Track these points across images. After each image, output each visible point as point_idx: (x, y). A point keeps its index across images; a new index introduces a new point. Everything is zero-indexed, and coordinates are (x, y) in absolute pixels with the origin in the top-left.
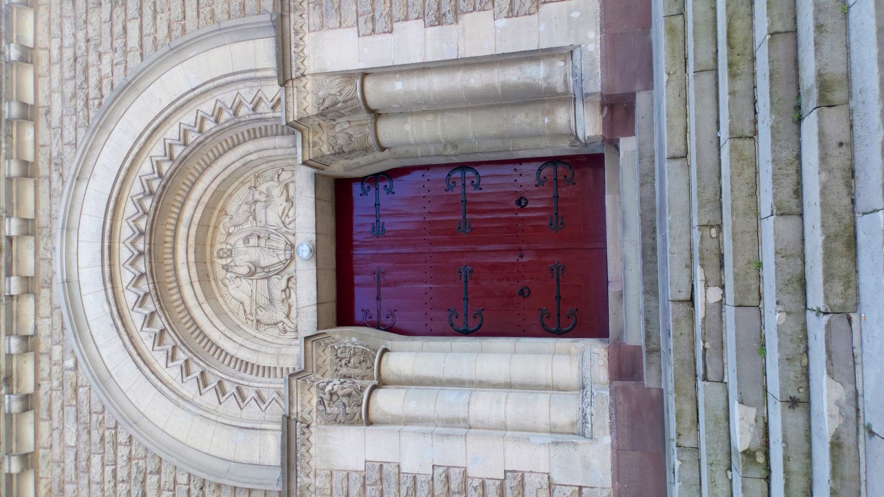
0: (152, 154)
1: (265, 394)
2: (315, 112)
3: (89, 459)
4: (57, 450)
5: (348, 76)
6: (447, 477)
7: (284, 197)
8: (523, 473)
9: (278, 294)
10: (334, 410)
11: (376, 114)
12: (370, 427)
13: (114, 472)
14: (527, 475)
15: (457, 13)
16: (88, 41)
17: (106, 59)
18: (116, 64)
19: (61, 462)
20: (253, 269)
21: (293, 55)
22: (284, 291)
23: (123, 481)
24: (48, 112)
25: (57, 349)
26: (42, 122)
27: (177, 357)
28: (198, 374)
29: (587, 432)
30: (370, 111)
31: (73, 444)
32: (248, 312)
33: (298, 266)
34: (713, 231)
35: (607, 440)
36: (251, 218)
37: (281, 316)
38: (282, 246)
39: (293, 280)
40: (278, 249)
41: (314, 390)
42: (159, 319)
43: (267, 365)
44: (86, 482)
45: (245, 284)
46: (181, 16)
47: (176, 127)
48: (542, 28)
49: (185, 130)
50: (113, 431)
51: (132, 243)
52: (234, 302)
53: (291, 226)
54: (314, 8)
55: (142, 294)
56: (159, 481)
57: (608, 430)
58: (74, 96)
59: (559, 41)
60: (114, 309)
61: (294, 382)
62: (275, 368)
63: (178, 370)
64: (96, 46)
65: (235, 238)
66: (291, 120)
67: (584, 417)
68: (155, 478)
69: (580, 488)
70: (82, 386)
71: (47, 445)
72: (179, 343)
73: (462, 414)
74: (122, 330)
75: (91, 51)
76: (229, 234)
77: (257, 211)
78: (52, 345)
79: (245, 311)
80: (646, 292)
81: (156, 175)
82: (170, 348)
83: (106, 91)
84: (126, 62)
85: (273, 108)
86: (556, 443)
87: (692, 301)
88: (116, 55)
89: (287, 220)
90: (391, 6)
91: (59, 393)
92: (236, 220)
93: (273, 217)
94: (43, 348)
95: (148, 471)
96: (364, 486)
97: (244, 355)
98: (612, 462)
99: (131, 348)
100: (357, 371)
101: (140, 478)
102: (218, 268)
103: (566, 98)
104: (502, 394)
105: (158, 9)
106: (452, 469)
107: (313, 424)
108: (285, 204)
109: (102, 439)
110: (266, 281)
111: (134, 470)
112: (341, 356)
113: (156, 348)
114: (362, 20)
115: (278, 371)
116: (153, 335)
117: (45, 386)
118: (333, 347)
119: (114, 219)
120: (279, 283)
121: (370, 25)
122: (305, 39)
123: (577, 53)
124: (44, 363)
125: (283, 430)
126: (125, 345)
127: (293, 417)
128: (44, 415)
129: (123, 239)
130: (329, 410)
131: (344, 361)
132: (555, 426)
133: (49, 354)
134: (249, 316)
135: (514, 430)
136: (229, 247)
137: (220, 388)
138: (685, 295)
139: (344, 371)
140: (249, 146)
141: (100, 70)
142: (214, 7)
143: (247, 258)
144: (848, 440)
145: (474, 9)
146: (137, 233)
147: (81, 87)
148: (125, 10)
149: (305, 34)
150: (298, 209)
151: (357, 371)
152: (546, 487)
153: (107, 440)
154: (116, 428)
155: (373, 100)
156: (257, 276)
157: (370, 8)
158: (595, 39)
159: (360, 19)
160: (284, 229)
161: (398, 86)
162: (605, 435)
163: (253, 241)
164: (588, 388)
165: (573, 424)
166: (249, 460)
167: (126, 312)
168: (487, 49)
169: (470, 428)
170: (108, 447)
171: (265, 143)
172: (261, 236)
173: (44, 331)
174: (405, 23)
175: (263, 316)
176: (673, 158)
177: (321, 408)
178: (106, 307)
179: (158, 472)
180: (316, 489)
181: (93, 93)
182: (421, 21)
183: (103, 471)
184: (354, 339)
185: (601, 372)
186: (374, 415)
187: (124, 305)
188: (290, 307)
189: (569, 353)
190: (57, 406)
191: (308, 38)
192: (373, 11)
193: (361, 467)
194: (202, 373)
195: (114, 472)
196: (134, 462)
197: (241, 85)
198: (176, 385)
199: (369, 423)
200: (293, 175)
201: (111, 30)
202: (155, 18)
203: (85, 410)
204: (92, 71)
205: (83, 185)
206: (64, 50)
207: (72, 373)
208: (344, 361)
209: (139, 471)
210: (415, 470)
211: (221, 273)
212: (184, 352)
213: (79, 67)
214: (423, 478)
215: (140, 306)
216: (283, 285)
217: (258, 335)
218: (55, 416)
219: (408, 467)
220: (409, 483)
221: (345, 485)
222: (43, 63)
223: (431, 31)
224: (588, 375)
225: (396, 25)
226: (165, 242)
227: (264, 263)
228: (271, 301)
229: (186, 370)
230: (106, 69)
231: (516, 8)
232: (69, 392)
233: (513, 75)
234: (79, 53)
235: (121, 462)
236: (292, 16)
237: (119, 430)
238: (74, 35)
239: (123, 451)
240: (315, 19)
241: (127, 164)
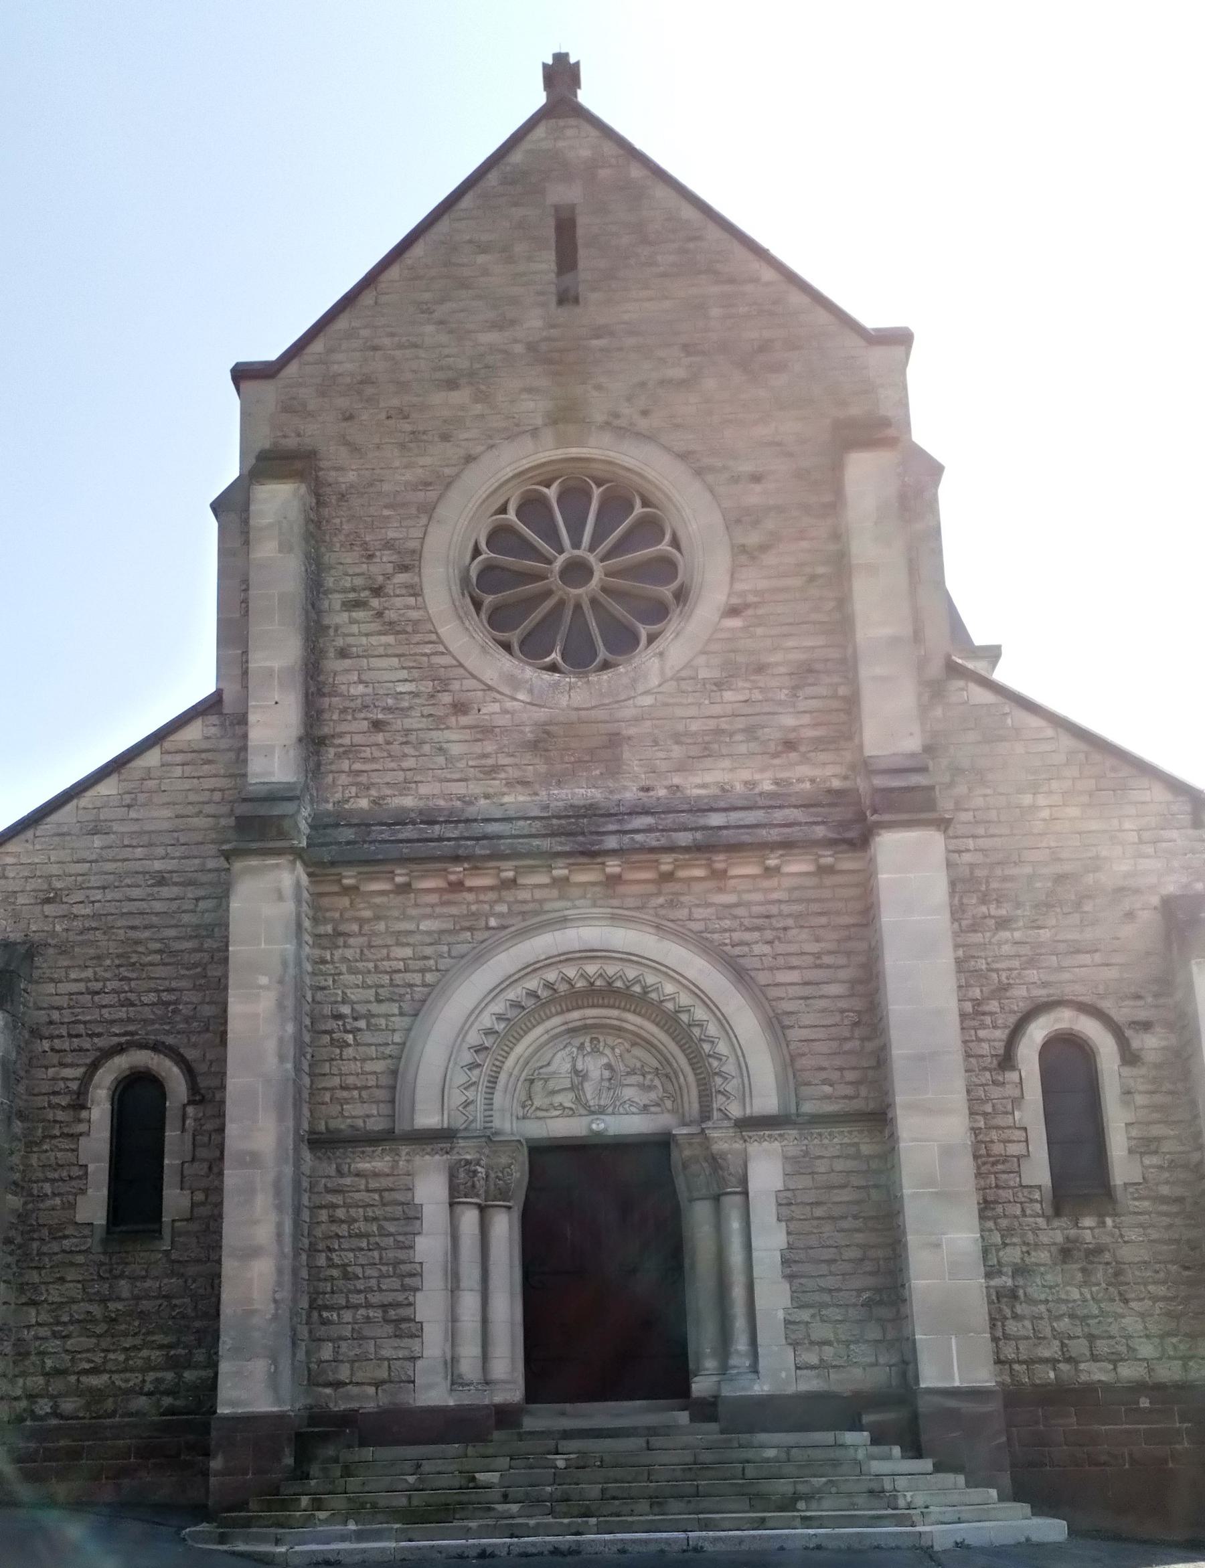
0: (681, 994)
1: (471, 1108)
3: (408, 944)
4: (413, 912)
5: (744, 1181)
6: (414, 1275)
7: (647, 1102)
11: (717, 1199)
13: (399, 971)
15: (790, 1277)
16: (785, 929)
17: (766, 949)
19: (405, 917)
22: (561, 1104)
23: (391, 980)
27: (501, 1022)
30: (719, 1196)
31: (421, 927)
32: (541, 1071)
34: (599, 1463)
35: (451, 1403)
37: (537, 1103)
38: (602, 1103)
39: (571, 1113)
40: (600, 1099)
41: (477, 1156)
44: (389, 943)
46: (801, 1024)
47: (705, 1018)
49: (702, 1025)
51: (601, 975)
53: (621, 1110)
54: (802, 1151)
55: (555, 987)
56: (393, 1015)
58: (735, 917)
59: (762, 1363)
61: (483, 1139)
63: (489, 1025)
64: (779, 938)
67: (468, 1385)
68: (396, 1011)
69: (413, 1382)
70: (472, 934)
73: (463, 1284)
74: (523, 973)
75: (774, 933)
76: (613, 1049)
80: (565, 1431)
82: (508, 1016)
84: (763, 970)
86: (446, 1363)
90: (801, 1220)
91: (465, 912)
92: (626, 1056)
93: (628, 1093)
94: (504, 893)
95: (402, 1004)
96: (403, 1204)
102: (581, 1040)
103: (724, 1369)
105: (809, 1002)
106: (419, 1278)
107: (449, 1157)
109: (426, 958)
111: (402, 991)
114: (789, 1194)
115: (490, 1113)
116: (519, 999)
117: (470, 897)
118: (512, 1164)
120: (566, 1099)
121: (784, 1202)
124: (491, 896)
126: (510, 976)
127: (455, 1140)
128: (446, 897)
129: (605, 967)
131: (500, 1175)
132: (458, 1361)
133: (500, 900)
134: (537, 1072)
136: (601, 1049)
137: (473, 1066)
139: (493, 1175)
140: (691, 1078)
141: (757, 942)
143: (591, 1067)
144: (492, 1514)
145: (793, 1292)
150: (640, 1116)
151: (492, 1187)
154: (437, 970)
155: (726, 1200)
157: (799, 1201)
158: (762, 1391)
160: (618, 1103)
162: (455, 1401)
163: (607, 1074)
165: (460, 1376)
168: (760, 1303)
169: (452, 1291)
171: (694, 1093)
172: (613, 1078)
173: (524, 895)
174: (784, 1232)
175: (538, 1085)
176: (648, 1442)
179: (401, 1014)
180: (397, 1162)
181: (737, 936)
184: (518, 1175)
186: (459, 1209)
187: (545, 970)
188: (547, 1110)
190: (454, 910)
191: (776, 1145)
192: (797, 1204)
193: (417, 1201)
194: (487, 1048)
195: (399, 971)
196: (408, 990)
197: (740, 1080)
198: (477, 1026)
199: (451, 1205)
200: (668, 1111)
201: (793, 954)
203: (451, 939)
204: (756, 935)
207: (483, 924)
208: (500, 1175)
209: (401, 995)
210: (418, 1247)
212: (504, 1028)
213: (759, 922)
214: (412, 1255)
217: (520, 1083)
218: (445, 910)
222: (767, 884)
223: (778, 1254)
224: (498, 1387)
225: (784, 1224)
227: (586, 1085)
230: (758, 949)
232: (467, 924)
234: (774, 921)
235: (408, 976)
238: (790, 915)
240: (792, 1151)
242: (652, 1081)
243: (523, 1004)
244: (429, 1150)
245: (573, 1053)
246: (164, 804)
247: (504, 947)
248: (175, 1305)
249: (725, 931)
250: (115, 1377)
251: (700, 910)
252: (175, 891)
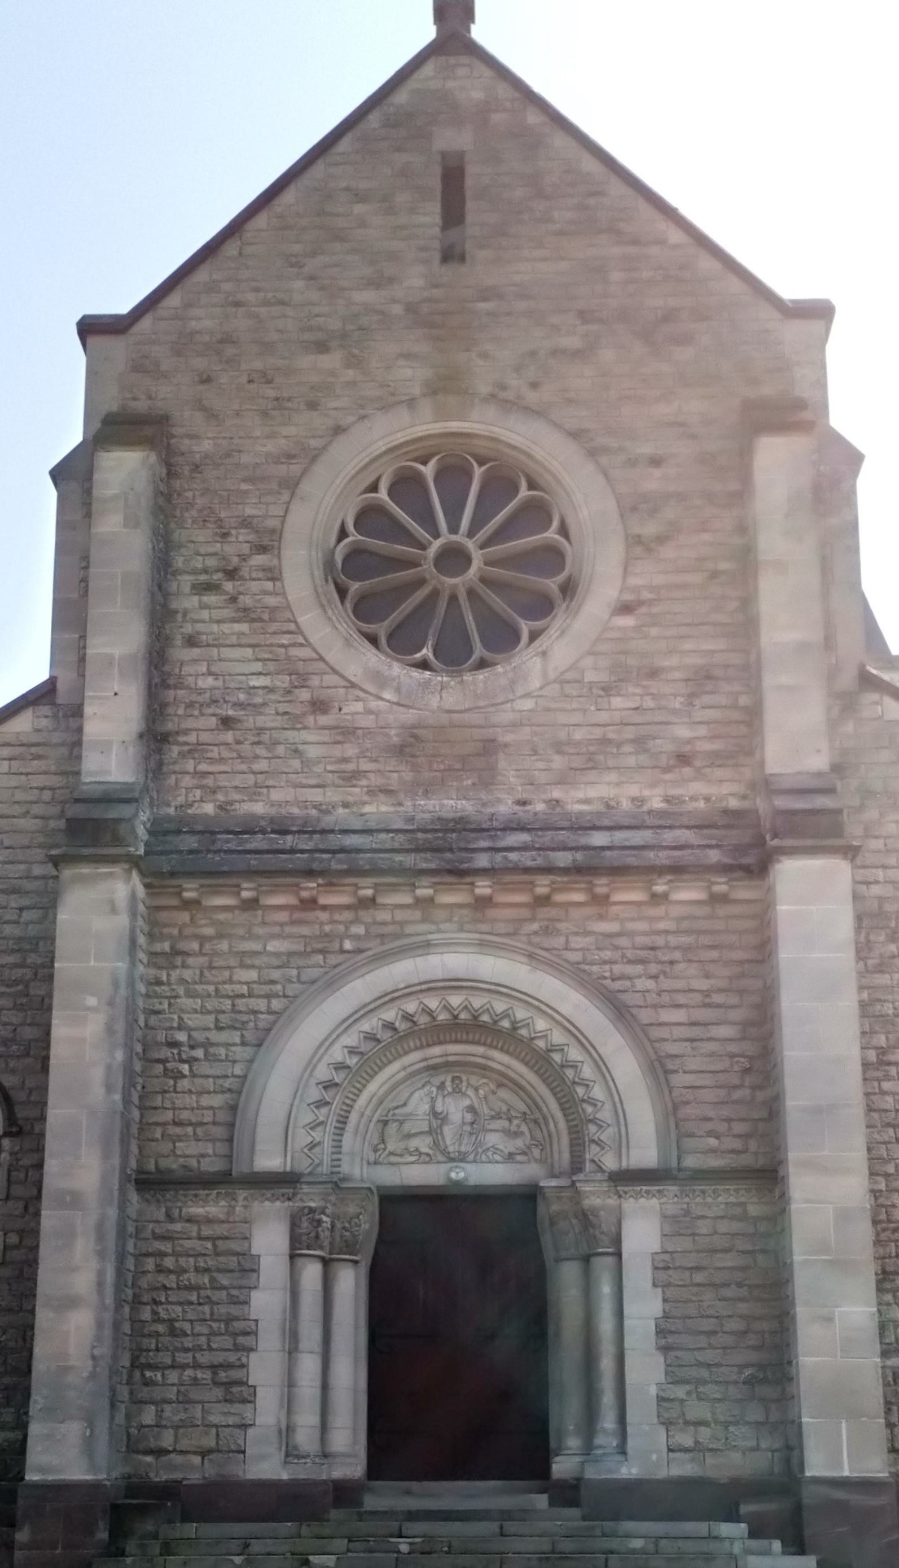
0: (554, 1030)
1: (317, 1150)
4: (260, 931)
5: (617, 1241)
6: (248, 1334)
7: (513, 1150)
8: (253, 1402)
9: (414, 1143)
10: (305, 1224)
11: (586, 1260)
12: (288, 1257)
13: (242, 996)
14: (252, 1405)
16: (672, 963)
17: (650, 984)
18: (644, 996)
19: (251, 936)
20: (441, 1116)
21: (639, 1188)
23: (233, 1005)
24: (601, 917)
27: (353, 1056)
28: (337, 1080)
29: (290, 1459)
31: (268, 948)
32: (396, 1111)
34: (446, 1549)
35: (285, 1476)
36: (493, 1113)
38: (463, 1149)
39: (428, 1159)
40: (460, 1145)
41: (322, 1204)
43: (344, 1143)
45: (426, 1107)
46: (687, 1069)
47: (580, 1058)
48: (646, 1428)
49: (576, 1067)
50: (281, 994)
52: (404, 1096)
54: (682, 1209)
55: (415, 1019)
56: (234, 1045)
57: (292, 1477)
58: (617, 948)
59: (631, 1443)
60: (400, 993)
61: (330, 1185)
63: (340, 1059)
64: (665, 973)
67: (304, 1457)
68: (238, 1040)
69: (244, 1452)
70: (325, 958)
71: (267, 919)
72: (366, 1057)
75: (660, 967)
76: (476, 1089)
78: (365, 924)
79: (396, 1108)
80: (410, 1512)
81: (533, 1035)
82: (362, 1050)
84: (646, 1007)
85: (593, 1161)
86: (280, 1432)
87: (401, 1537)
88: (654, 996)
89: (490, 1154)
91: (318, 933)
92: (491, 1097)
94: (362, 913)
95: (244, 1032)
96: (238, 1254)
97: (354, 1117)
99: (362, 1012)
100: (338, 1239)
101: (237, 1025)
102: (442, 1078)
103: (588, 1448)
104: (318, 1383)
105: (695, 1044)
107: (291, 1203)
108: (506, 1151)
109: (273, 982)
110: (427, 1129)
112: (353, 1224)
113: (362, 1035)
117: (324, 916)
118: (361, 1213)
119: (489, 991)
120: (423, 1144)
121: (661, 1265)
123: (622, 1458)
124: (347, 915)
126: (365, 1006)
127: (298, 1185)
128: (297, 915)
130: (304, 1218)
131: (347, 1225)
132: (294, 1431)
133: (357, 921)
134: (391, 1113)
135: (289, 1392)
136: (464, 1089)
137: (321, 1104)
139: (339, 1225)
140: (562, 1124)
141: (640, 977)
143: (452, 1110)
146: (476, 1014)
147: (623, 956)
151: (338, 1239)
152: (243, 1422)
153: (272, 987)
154: (285, 996)
156: (433, 1121)
157: (677, 1264)
158: (630, 1474)
160: (480, 1150)
161: (606, 1289)
163: (469, 1117)
164: (325, 1461)
165: (296, 1448)
167: (398, 1002)
170: (266, 989)
171: (565, 1141)
172: (476, 1123)
175: (393, 1127)
177: (306, 1211)
178: (402, 985)
179: (243, 1044)
180: (234, 1207)
181: (617, 969)
183: (243, 983)
187: (403, 1000)
188: (401, 1155)
190: (305, 930)
191: (654, 1202)
192: (675, 1268)
193: (254, 1252)
194: (336, 1085)
195: (242, 996)
196: (252, 1017)
197: (616, 1129)
198: (327, 1059)
199: (292, 1257)
202: (687, 1040)
203: (301, 962)
204: (639, 968)
205: (524, 960)
207: (337, 946)
209: (244, 1023)
211: (437, 1081)
212: (357, 1063)
217: (372, 1124)
220: (242, 1298)
221: (238, 1235)
223: (653, 1324)
225: (659, 1290)
226: (467, 1033)
228: (409, 1136)
229: (340, 1067)
230: (641, 984)
231: (665, 1404)
233: (608, 1399)
234: (659, 953)
237: (282, 999)
238: (677, 948)
239: (261, 1004)
241: (544, 1007)
242: (518, 1126)
243: (379, 1036)
244: (269, 1195)
245: (432, 1092)
249: (605, 962)
251: (579, 939)
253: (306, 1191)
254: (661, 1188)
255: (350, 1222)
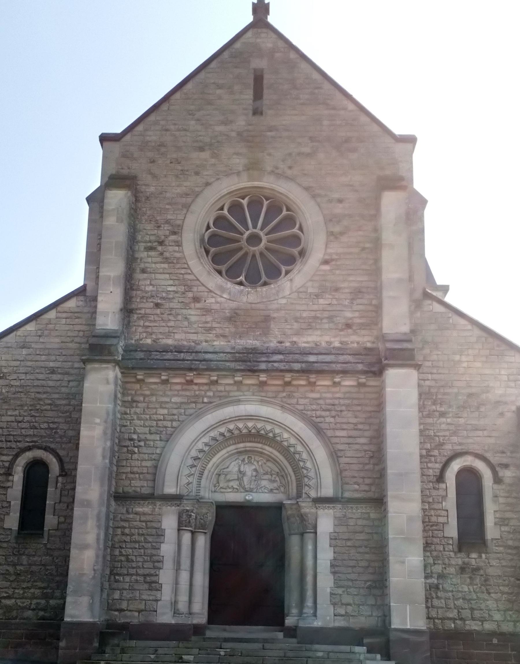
1: (190, 486)
2: (302, 513)
3: (165, 408)
4: (169, 393)
5: (315, 527)
8: (161, 590)
9: (231, 484)
10: (184, 516)
11: (302, 535)
13: (161, 420)
14: (160, 592)
15: (334, 573)
16: (341, 411)
17: (332, 420)
19: (165, 395)
20: (242, 473)
21: (325, 505)
23: (157, 424)
24: (312, 391)
25: (210, 394)
26: (307, 388)
30: (303, 533)
32: (224, 470)
33: (243, 493)
34: (240, 654)
35: (173, 622)
36: (265, 472)
37: (221, 485)
38: (252, 487)
39: (237, 491)
40: (250, 485)
41: (192, 508)
42: (222, 438)
43: (202, 483)
45: (236, 469)
47: (301, 450)
48: (325, 606)
49: (300, 454)
50: (177, 420)
54: (343, 514)
55: (233, 432)
56: (157, 440)
57: (176, 622)
58: (318, 404)
59: (319, 612)
60: (227, 421)
62: (200, 487)
63: (201, 448)
64: (338, 415)
65: (256, 465)
66: (299, 503)
67: (181, 614)
68: (158, 439)
69: (156, 611)
70: (196, 405)
71: (172, 388)
73: (182, 568)
74: (218, 424)
75: (336, 413)
76: (258, 462)
77: (268, 476)
79: (224, 469)
80: (225, 638)
81: (282, 440)
82: (210, 444)
83: (318, 420)
84: (330, 429)
87: (221, 649)
88: (334, 425)
89: (263, 489)
90: (340, 547)
92: (264, 465)
94: (212, 387)
96: (156, 528)
98: (165, 623)
102: (243, 457)
103: (301, 613)
105: (350, 445)
106: (162, 563)
108: (270, 488)
109: (174, 415)
110: (237, 478)
112: (205, 517)
114: (336, 534)
116: (216, 437)
117: (196, 387)
118: (208, 513)
120: (235, 484)
121: (333, 538)
122: (331, 510)
123: (314, 618)
124: (206, 388)
125: (177, 495)
126: (212, 426)
127: (182, 500)
128: (184, 387)
131: (202, 517)
132: (177, 603)
133: (210, 390)
134: (222, 471)
136: (253, 462)
137: (193, 466)
138: (222, 648)
139: (199, 517)
140: (293, 478)
141: (328, 417)
142: (349, 470)
143: (247, 470)
146: (259, 430)
148: (352, 430)
149: (333, 510)
150: (269, 494)
151: (198, 523)
152: (156, 599)
153: (173, 417)
154: (179, 421)
158: (318, 625)
159: (336, 534)
160: (259, 488)
161: (310, 547)
163: (254, 473)
164: (190, 616)
165: (178, 610)
166: (166, 480)
167: (226, 425)
171: (295, 485)
173: (221, 388)
175: (222, 477)
176: (263, 646)
177: (185, 511)
178: (228, 418)
179: (161, 440)
180: (155, 509)
181: (318, 413)
182: (333, 558)
185: (196, 621)
187: (228, 424)
188: (225, 489)
189: (203, 609)
190: (188, 393)
191: (331, 511)
192: (339, 539)
193: (163, 527)
194: (199, 458)
195: (161, 420)
196: (165, 429)
197: (316, 480)
198: (195, 448)
199: (179, 530)
202: (347, 444)
205: (279, 408)
206: (338, 400)
209: (161, 431)
210: (162, 549)
212: (208, 450)
213: (329, 407)
215: (228, 430)
216: (235, 487)
217: (214, 476)
219: (163, 545)
220: (157, 547)
221: (156, 520)
223: (329, 562)
225: (332, 548)
226: (255, 438)
228: (229, 481)
229: (201, 451)
230: (328, 420)
231: (333, 596)
232: (194, 400)
233: (309, 593)
234: (336, 407)
236: (340, 506)
239: (169, 424)
242: (275, 478)
243: (218, 439)
244: (170, 504)
245: (239, 463)
246: (56, 336)
247: (210, 412)
248: (48, 569)
249: (313, 410)
250: (18, 601)
251: (302, 400)
252: (59, 377)
253: (185, 502)
254: (334, 505)
255: (203, 516)
